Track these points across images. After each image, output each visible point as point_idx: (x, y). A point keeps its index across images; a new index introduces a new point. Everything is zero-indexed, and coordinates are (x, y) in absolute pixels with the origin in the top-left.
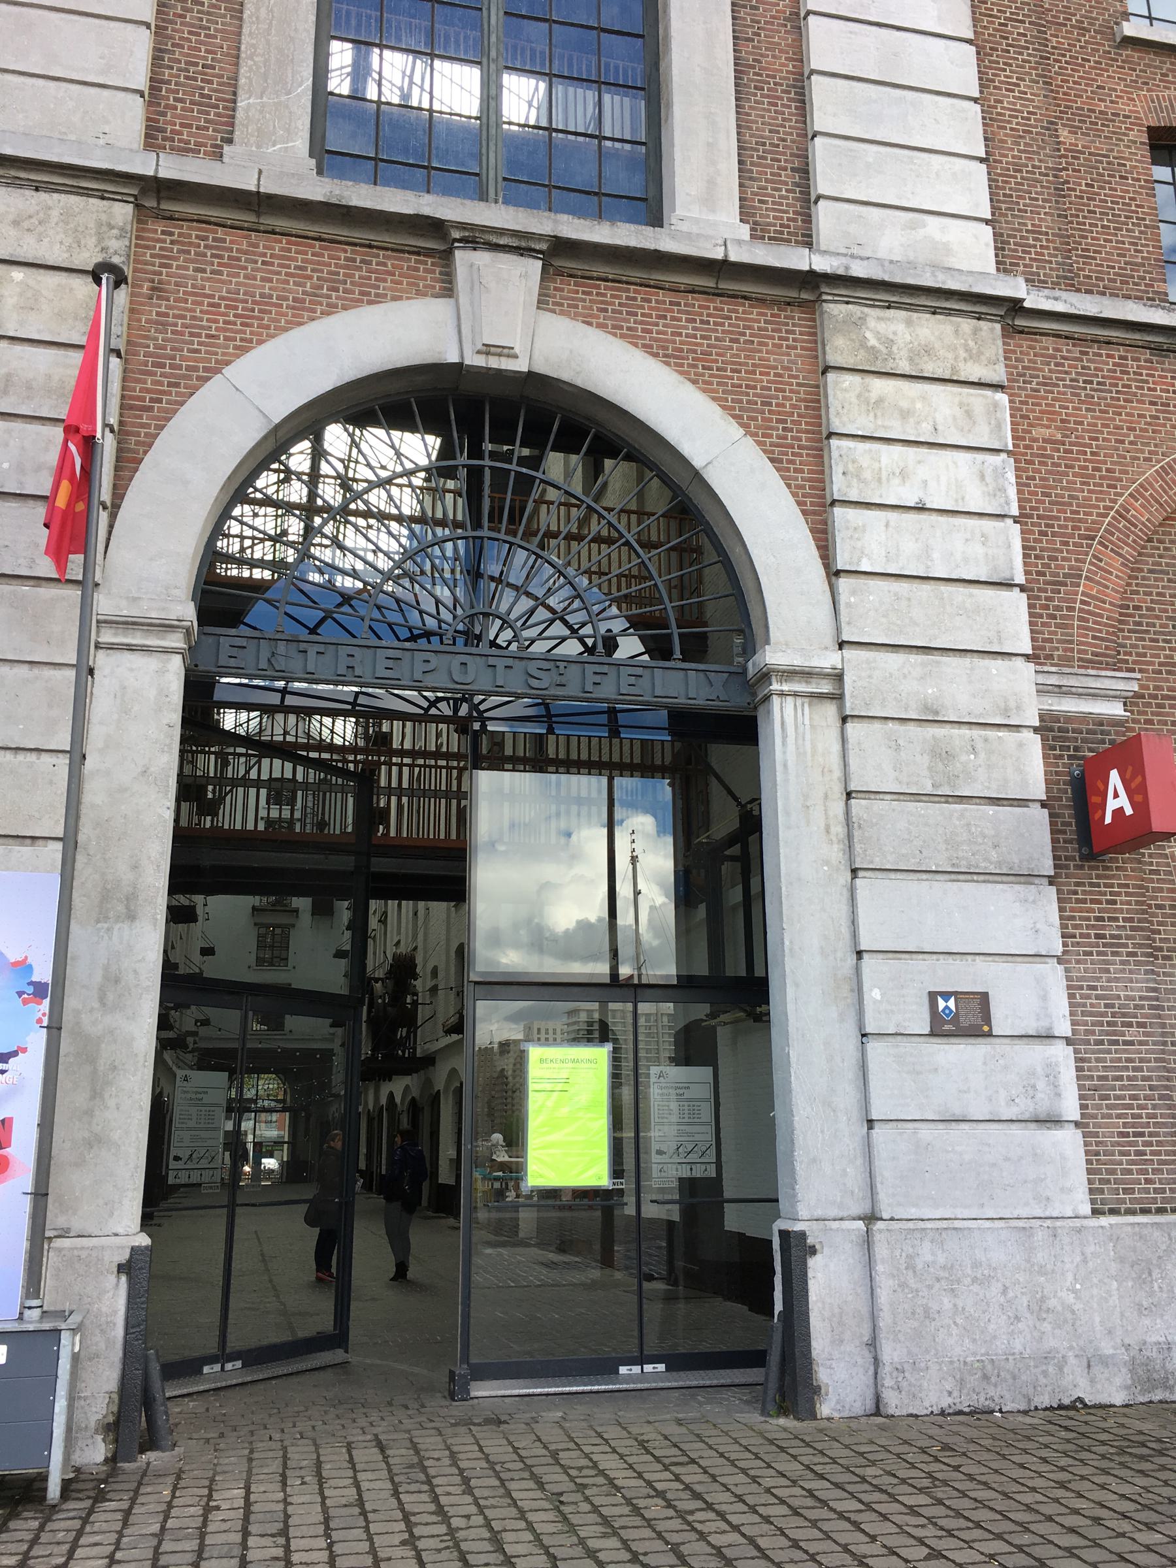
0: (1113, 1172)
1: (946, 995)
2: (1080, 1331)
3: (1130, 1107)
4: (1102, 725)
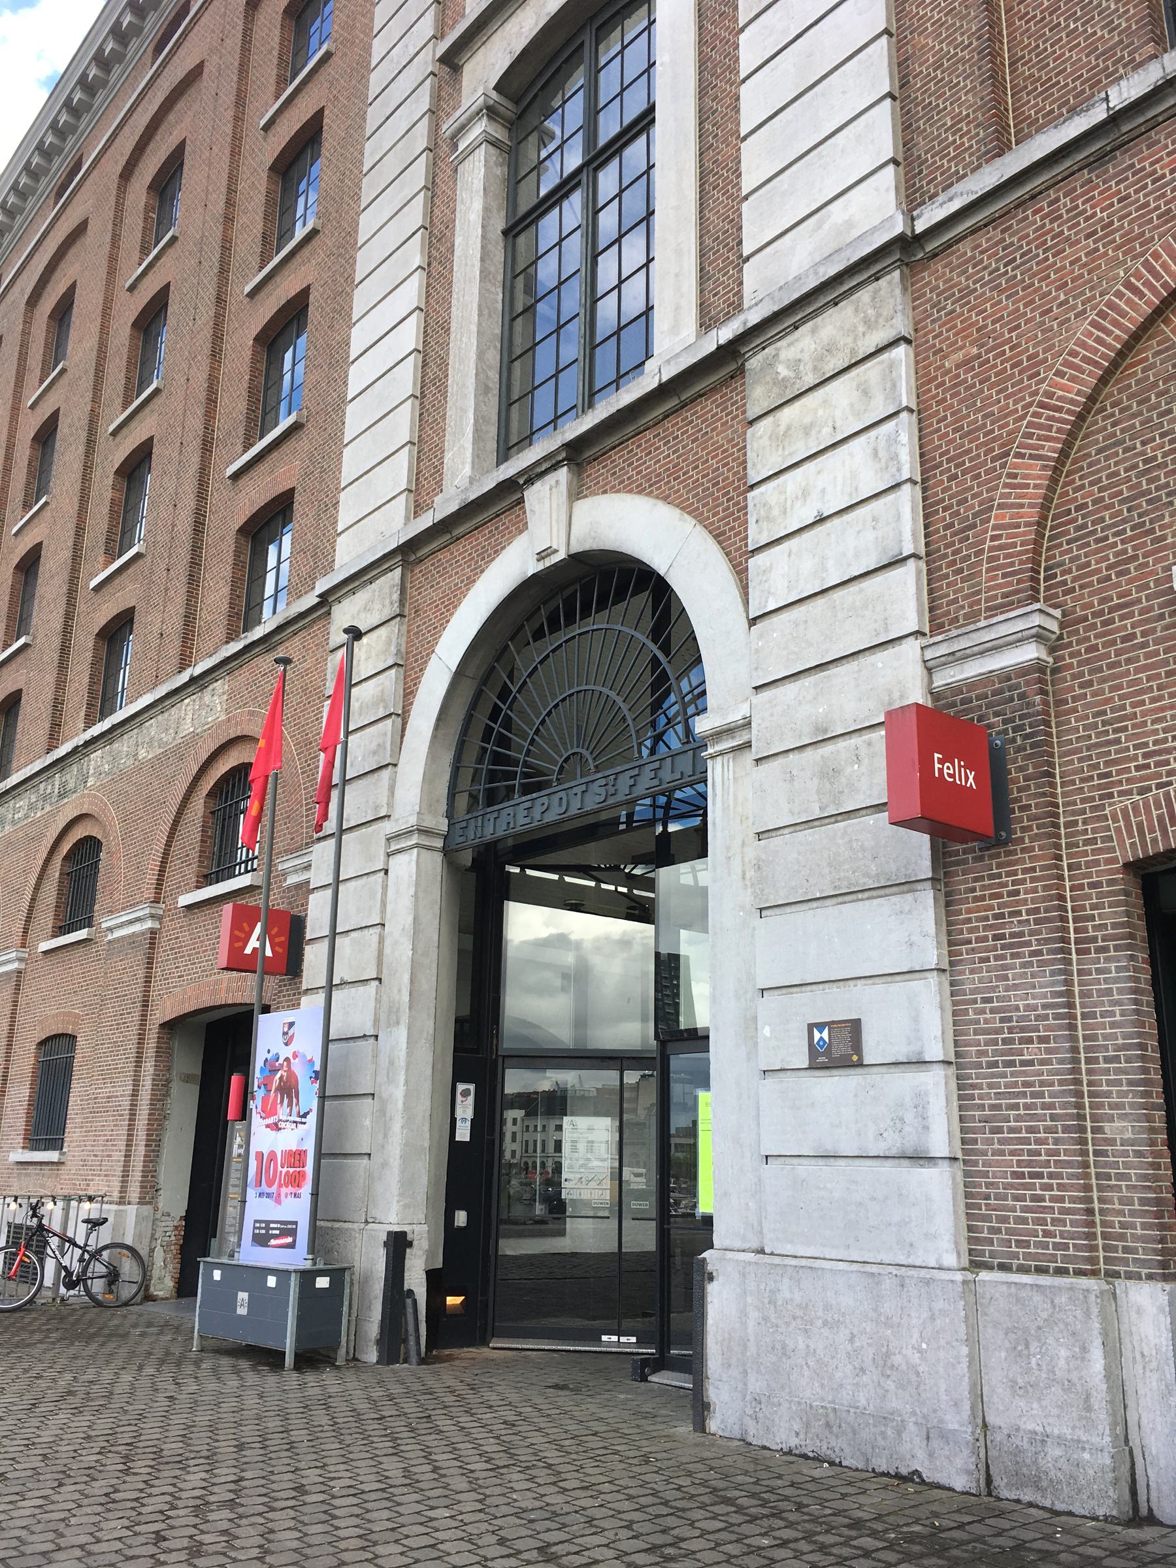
0: (1005, 1220)
1: (820, 1026)
2: (923, 1395)
3: (1026, 1141)
4: (1009, 679)
